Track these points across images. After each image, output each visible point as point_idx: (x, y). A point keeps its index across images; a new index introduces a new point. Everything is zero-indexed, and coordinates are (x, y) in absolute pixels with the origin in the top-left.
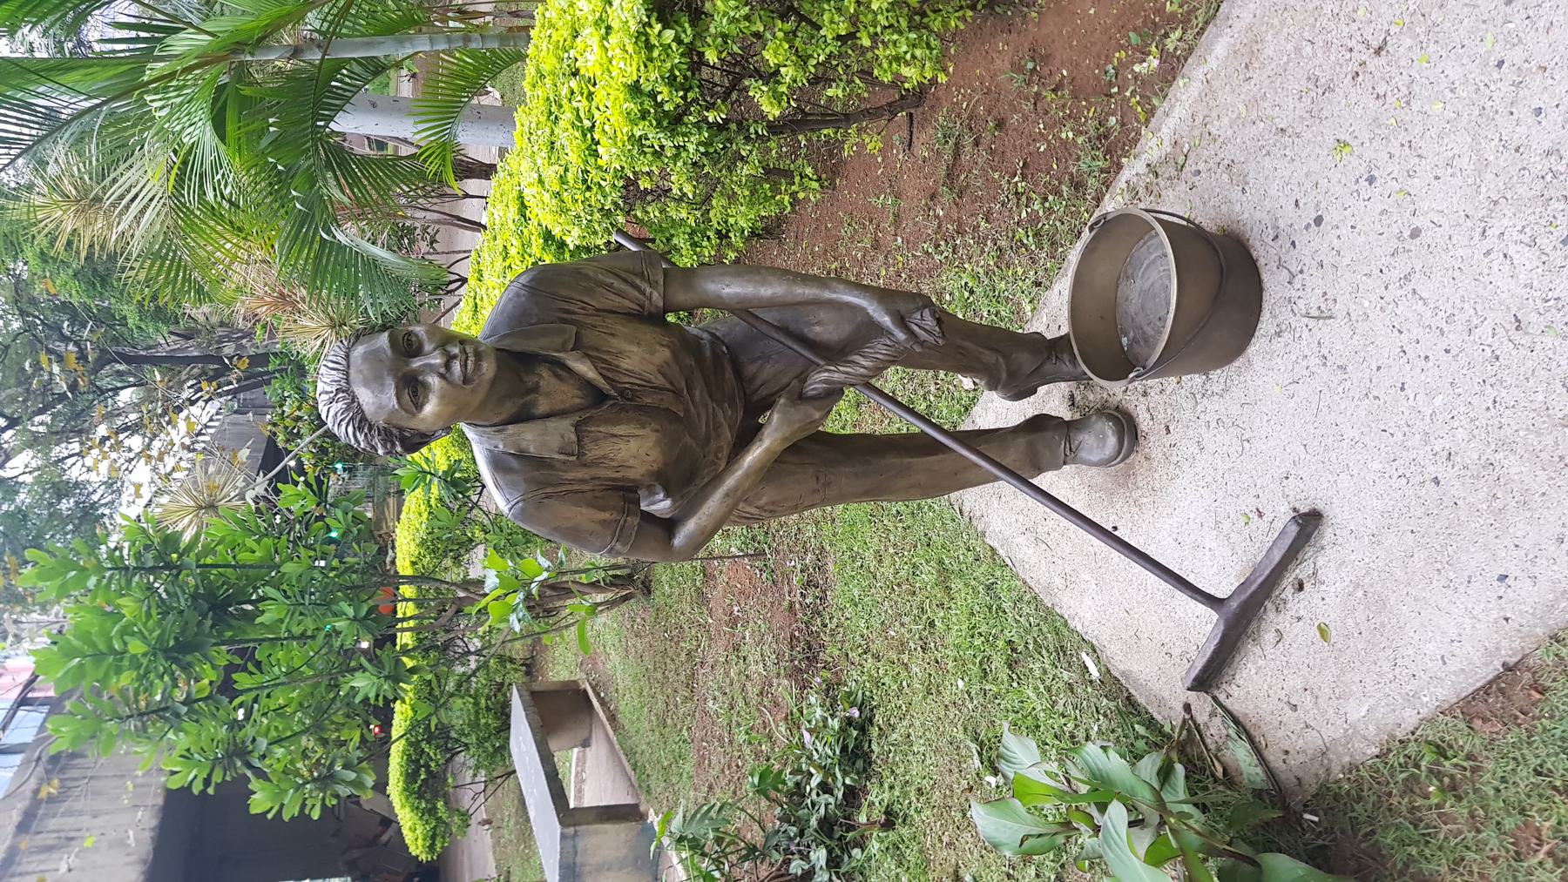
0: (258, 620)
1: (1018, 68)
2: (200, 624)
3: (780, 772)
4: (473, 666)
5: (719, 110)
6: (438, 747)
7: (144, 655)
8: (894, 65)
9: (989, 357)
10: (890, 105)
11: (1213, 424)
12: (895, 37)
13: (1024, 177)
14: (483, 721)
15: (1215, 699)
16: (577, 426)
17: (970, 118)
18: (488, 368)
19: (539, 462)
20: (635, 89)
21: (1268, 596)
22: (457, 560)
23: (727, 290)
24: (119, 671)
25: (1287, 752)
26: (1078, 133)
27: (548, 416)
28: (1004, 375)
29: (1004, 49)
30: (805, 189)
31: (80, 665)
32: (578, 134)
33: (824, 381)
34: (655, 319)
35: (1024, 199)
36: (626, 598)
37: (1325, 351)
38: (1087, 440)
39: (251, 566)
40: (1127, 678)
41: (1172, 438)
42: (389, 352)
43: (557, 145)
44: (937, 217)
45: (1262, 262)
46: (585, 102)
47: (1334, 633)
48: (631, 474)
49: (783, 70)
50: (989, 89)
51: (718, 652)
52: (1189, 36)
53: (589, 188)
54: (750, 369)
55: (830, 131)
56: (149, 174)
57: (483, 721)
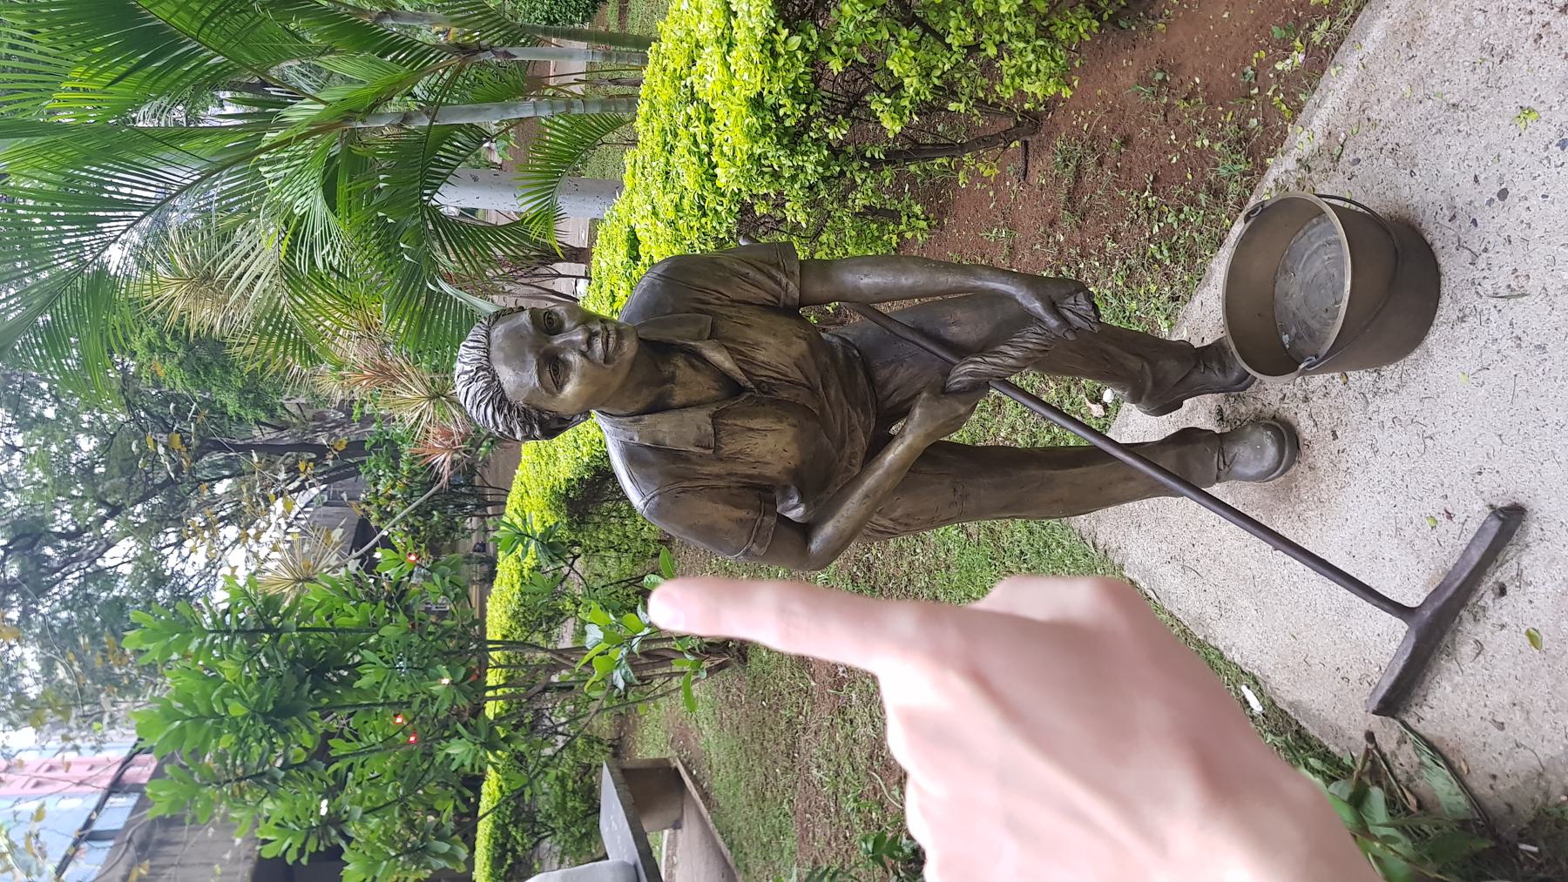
0: (357, 684)
1: (1147, 82)
2: (297, 688)
3: (895, 839)
4: (561, 745)
5: (840, 126)
6: (524, 831)
7: (244, 718)
8: (1017, 80)
9: (1134, 364)
10: (1005, 132)
11: (1388, 424)
12: (1022, 45)
13: (1154, 191)
14: (570, 804)
15: (1404, 724)
16: (714, 417)
17: (1093, 139)
18: (629, 347)
19: (675, 456)
20: (757, 103)
21: (1463, 605)
22: (547, 635)
23: (866, 280)
24: (219, 734)
25: (1494, 777)
26: (1213, 140)
27: (684, 407)
28: (1149, 384)
29: (1127, 69)
30: (913, 229)
31: (182, 728)
32: (695, 159)
33: (970, 374)
34: (789, 311)
35: (1155, 213)
36: (721, 667)
37: (1518, 332)
38: (1242, 452)
39: (350, 631)
40: (1296, 712)
41: (1339, 444)
42: (531, 328)
43: (673, 174)
44: (1057, 243)
45: (1438, 245)
46: (703, 128)
47: (1545, 638)
48: (769, 471)
49: (907, 81)
50: (1112, 107)
51: (822, 716)
52: (1339, 23)
53: (705, 215)
54: (883, 374)
55: (945, 161)
56: (264, 245)
57: (570, 804)
